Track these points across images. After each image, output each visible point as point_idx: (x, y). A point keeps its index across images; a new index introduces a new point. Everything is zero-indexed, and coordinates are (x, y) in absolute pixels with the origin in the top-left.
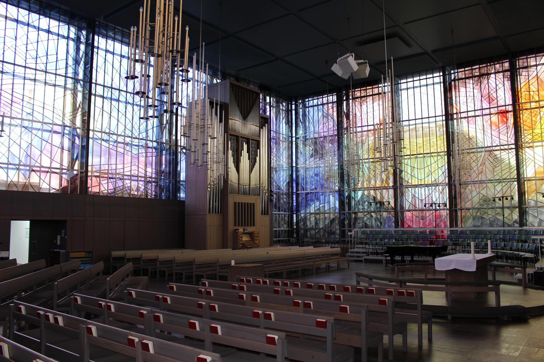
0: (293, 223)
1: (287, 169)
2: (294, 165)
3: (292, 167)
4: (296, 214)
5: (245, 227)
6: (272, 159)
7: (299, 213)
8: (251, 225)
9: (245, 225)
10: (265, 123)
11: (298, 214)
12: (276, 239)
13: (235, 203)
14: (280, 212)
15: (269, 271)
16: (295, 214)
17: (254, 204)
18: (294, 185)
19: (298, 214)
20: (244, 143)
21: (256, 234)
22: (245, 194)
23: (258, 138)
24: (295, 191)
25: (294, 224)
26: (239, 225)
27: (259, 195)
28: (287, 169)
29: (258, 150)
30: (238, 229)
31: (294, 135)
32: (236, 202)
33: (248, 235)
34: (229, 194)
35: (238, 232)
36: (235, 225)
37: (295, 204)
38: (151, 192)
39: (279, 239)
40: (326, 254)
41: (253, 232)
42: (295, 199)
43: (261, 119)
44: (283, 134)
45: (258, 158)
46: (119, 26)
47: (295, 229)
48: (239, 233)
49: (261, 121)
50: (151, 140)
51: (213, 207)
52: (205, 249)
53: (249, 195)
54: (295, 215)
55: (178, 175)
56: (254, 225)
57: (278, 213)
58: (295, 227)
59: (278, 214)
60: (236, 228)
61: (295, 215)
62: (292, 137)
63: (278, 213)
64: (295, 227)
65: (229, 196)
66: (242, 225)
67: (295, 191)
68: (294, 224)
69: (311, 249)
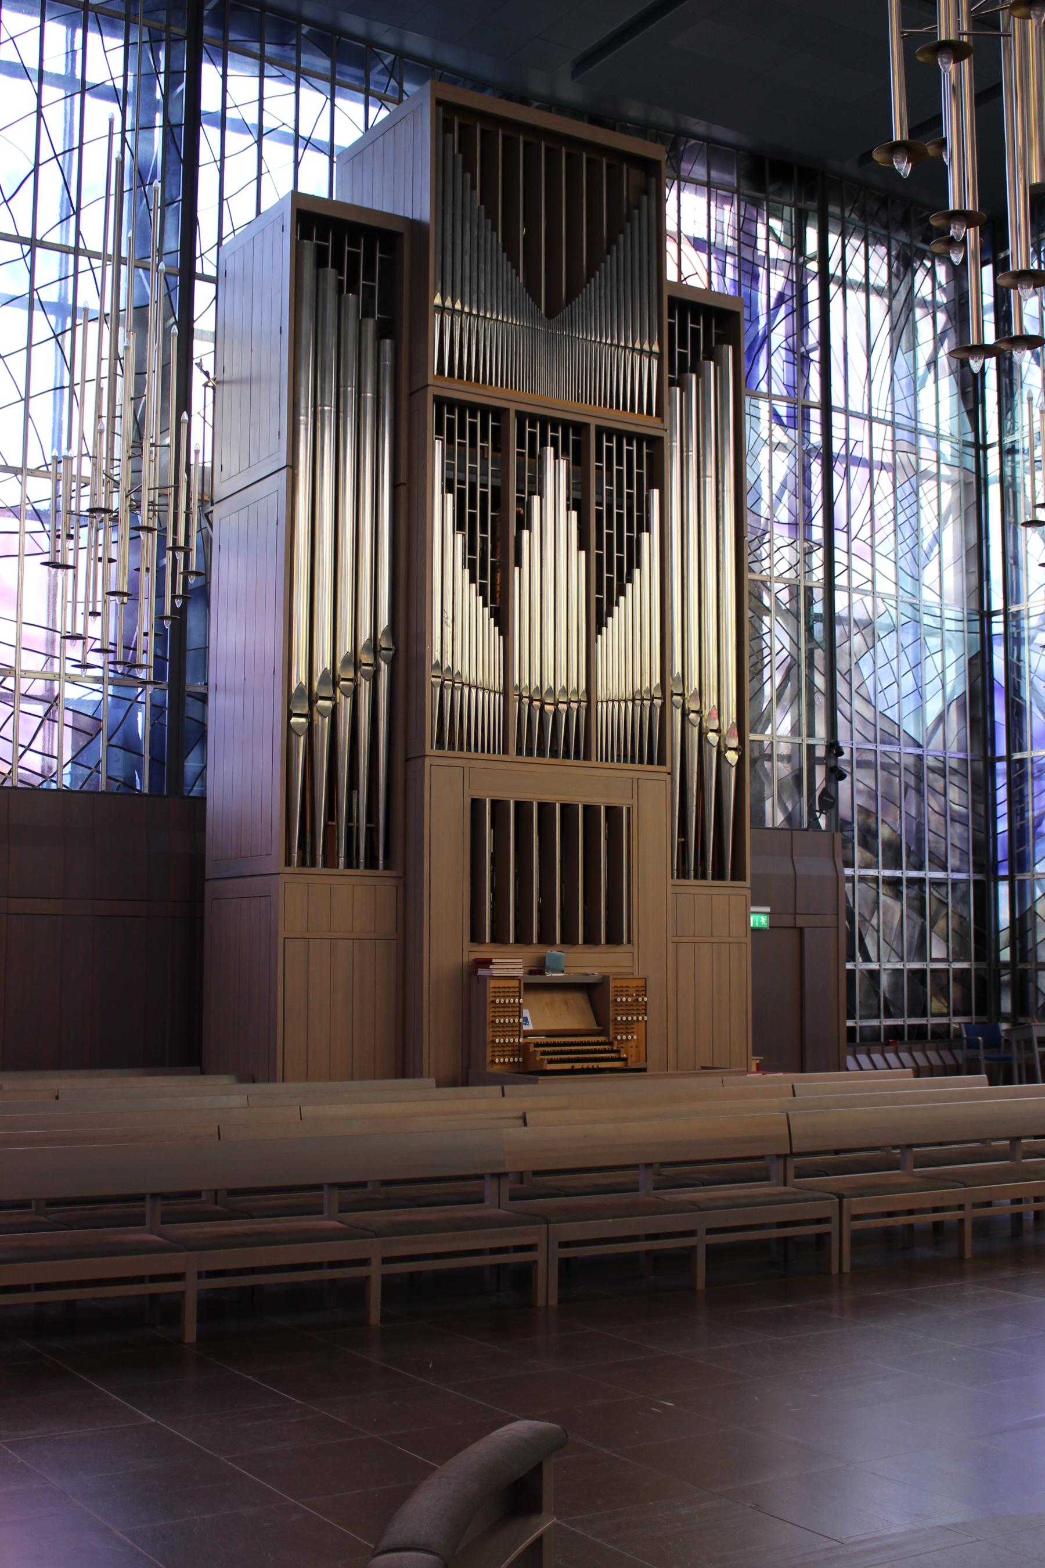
0: (998, 932)
1: (960, 626)
2: (997, 604)
3: (985, 616)
4: (1011, 879)
5: (553, 952)
6: (838, 569)
7: (1026, 876)
8: (591, 939)
9: (545, 938)
10: (723, 340)
11: (1022, 882)
12: (874, 1022)
13: (476, 804)
14: (921, 868)
15: (710, 1231)
16: (1004, 878)
17: (613, 812)
18: (1000, 715)
19: (1022, 882)
20: (550, 451)
21: (621, 991)
22: (452, 747)
23: (653, 420)
24: (1001, 749)
25: (1004, 936)
26: (499, 937)
27: (662, 762)
28: (960, 626)
29: (656, 493)
30: (487, 963)
31: (993, 436)
32: (478, 794)
33: (578, 1000)
34: (428, 751)
35: (485, 978)
36: (476, 936)
37: (1002, 826)
38: (15, 751)
39: (898, 1022)
40: (879, 1144)
41: (604, 982)
42: (1002, 794)
43: (671, 316)
44: (938, 436)
45: (649, 543)
46: (623, 195)
47: (1005, 965)
48: (493, 983)
49: (671, 326)
50: (16, 462)
51: (371, 833)
52: (271, 1078)
53: (587, 757)
54: (1003, 889)
55: (190, 656)
56: (614, 938)
57: (888, 873)
58: (1005, 955)
59: (911, 881)
60: (482, 952)
61: (1003, 889)
62: (980, 447)
63: (888, 873)
64: (1005, 955)
65: (428, 761)
66: (522, 938)
67: (1001, 749)
68: (1004, 936)
69: (975, 1096)
